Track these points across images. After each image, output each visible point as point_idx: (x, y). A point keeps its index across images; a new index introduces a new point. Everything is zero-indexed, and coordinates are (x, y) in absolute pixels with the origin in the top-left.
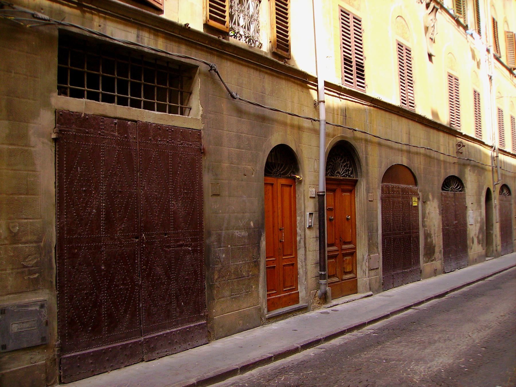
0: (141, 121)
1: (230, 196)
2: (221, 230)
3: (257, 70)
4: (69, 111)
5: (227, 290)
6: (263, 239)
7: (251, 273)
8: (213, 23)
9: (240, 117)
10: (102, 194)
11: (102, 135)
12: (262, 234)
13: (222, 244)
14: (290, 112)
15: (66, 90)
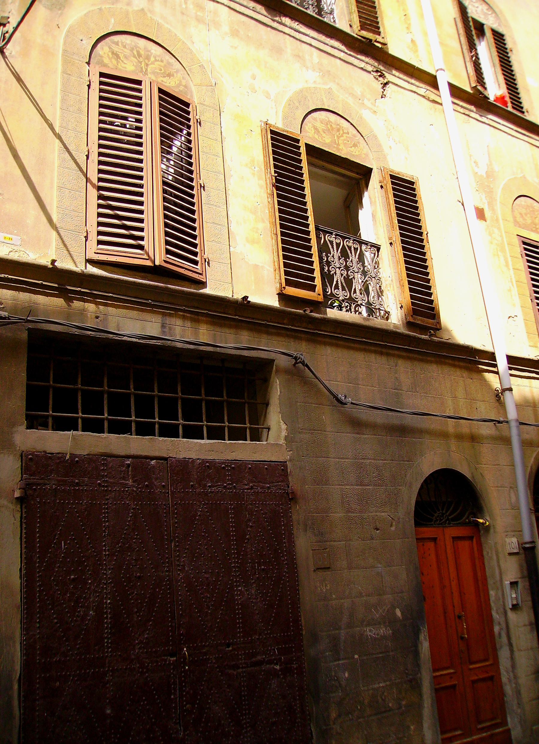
0: (175, 458)
1: (350, 568)
2: (337, 629)
3: (381, 354)
4: (45, 452)
5: (358, 739)
6: (423, 638)
7: (404, 703)
8: (292, 291)
9: (358, 433)
10: (105, 584)
11: (103, 486)
12: (420, 629)
13: (342, 654)
14: (452, 414)
15: (250, 303)
